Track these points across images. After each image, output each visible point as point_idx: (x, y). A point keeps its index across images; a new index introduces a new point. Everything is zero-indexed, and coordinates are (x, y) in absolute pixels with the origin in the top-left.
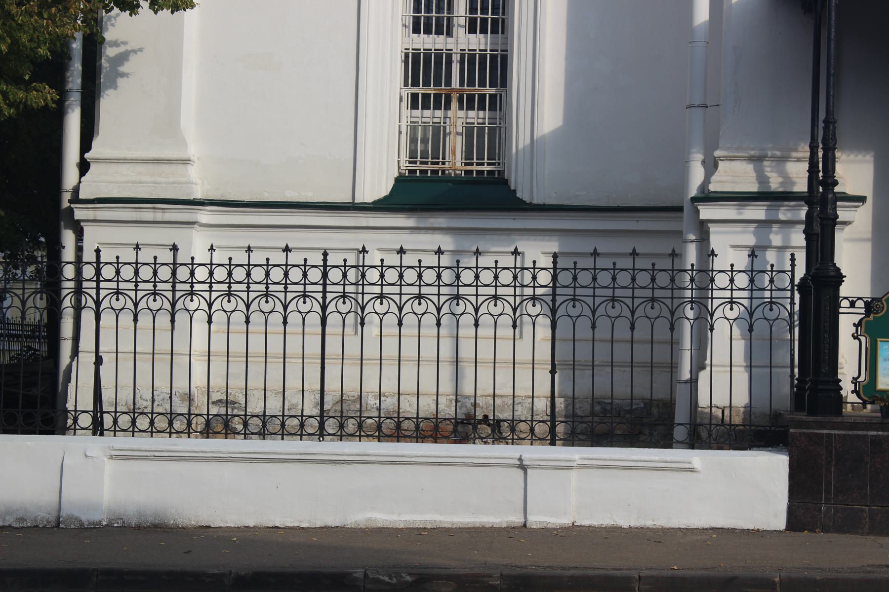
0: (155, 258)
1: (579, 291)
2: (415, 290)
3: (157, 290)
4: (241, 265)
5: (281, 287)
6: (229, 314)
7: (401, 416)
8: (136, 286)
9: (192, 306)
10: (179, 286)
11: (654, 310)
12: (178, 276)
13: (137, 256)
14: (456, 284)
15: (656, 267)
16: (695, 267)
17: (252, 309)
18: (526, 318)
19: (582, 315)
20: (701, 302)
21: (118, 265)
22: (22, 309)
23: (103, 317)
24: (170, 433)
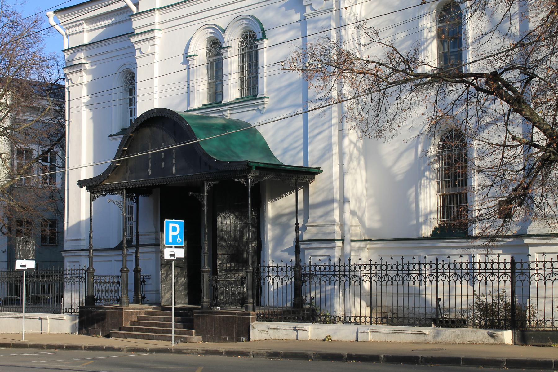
1: (494, 271)
8: (381, 272)
23: (404, 283)
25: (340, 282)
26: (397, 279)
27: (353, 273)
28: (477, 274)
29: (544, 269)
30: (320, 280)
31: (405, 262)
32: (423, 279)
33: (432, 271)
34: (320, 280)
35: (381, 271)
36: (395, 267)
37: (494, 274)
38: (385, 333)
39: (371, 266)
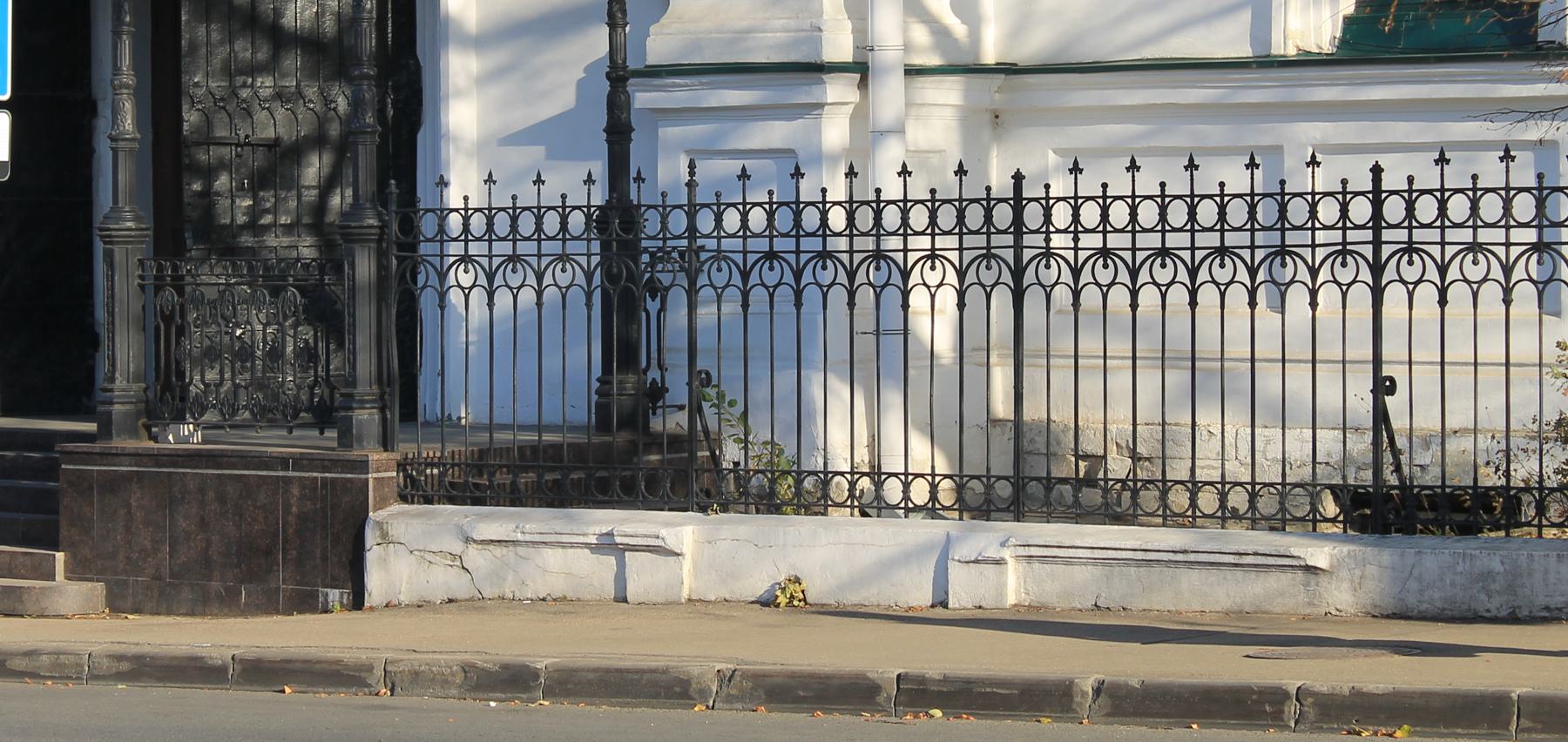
0: (1105, 186)
4: (1494, 190)
7: (1448, 483)
8: (1076, 240)
9: (826, 277)
10: (1386, 235)
11: (1479, 266)
13: (1133, 181)
14: (1309, 225)
15: (938, 196)
16: (775, 196)
17: (1451, 276)
20: (946, 255)
21: (1410, 198)
24: (1224, 519)
26: (1223, 276)
31: (550, 196)
33: (1352, 236)
35: (1076, 232)
39: (1377, 197)
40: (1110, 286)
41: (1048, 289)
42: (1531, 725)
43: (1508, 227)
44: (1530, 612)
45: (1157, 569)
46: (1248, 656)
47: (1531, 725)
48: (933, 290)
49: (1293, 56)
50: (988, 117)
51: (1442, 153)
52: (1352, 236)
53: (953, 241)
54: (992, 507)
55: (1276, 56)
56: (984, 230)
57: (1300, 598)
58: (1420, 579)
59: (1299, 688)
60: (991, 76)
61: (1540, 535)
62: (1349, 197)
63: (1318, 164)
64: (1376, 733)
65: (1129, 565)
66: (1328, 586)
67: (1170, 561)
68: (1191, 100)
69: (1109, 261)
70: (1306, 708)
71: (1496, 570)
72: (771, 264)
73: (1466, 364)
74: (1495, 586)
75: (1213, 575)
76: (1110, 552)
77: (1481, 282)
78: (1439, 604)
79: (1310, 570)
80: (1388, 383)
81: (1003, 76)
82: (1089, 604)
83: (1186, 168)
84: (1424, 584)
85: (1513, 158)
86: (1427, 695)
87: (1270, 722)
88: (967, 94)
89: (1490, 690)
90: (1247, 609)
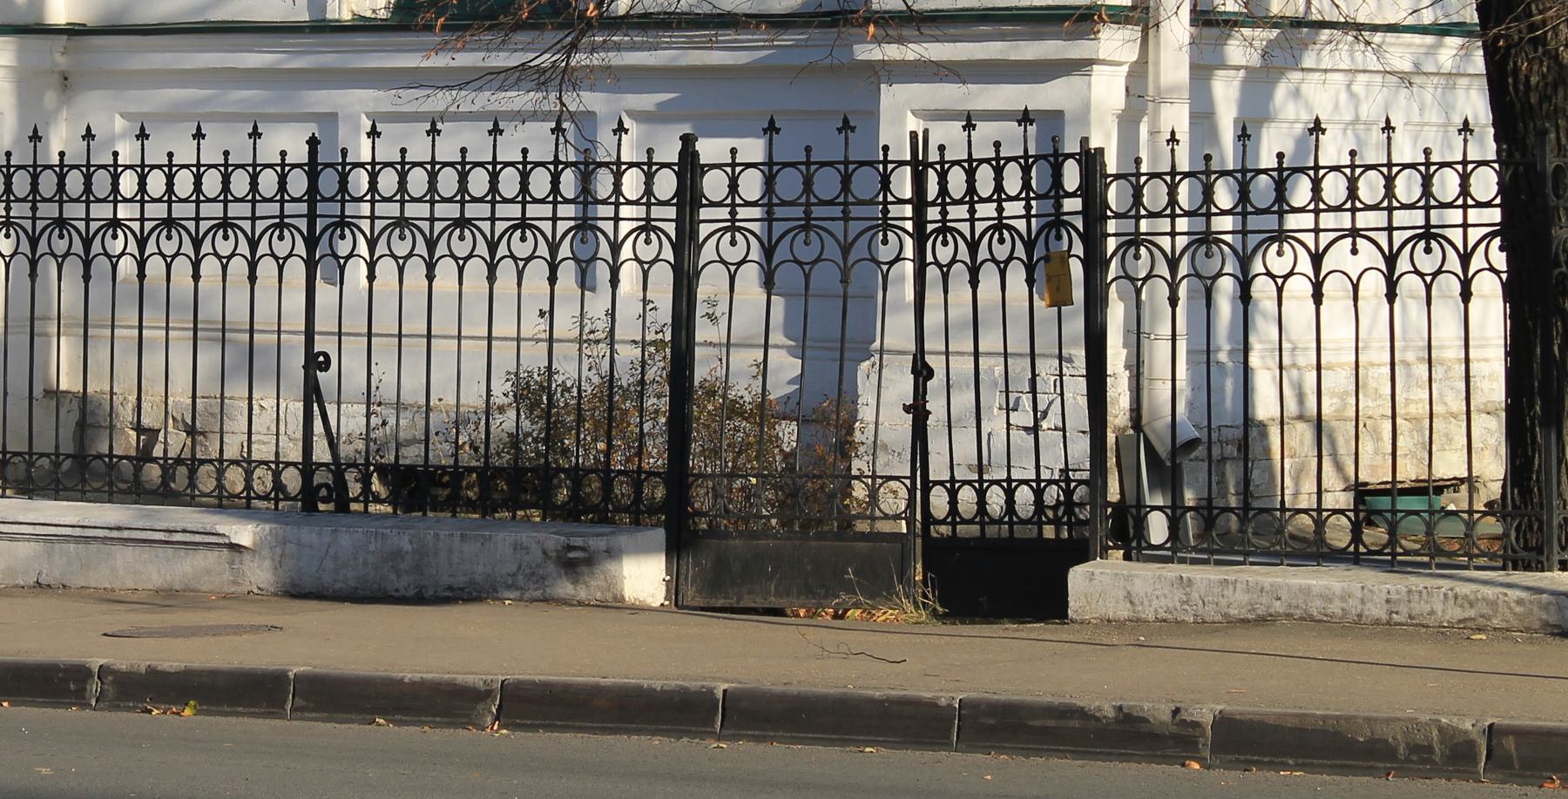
0: (170, 155)
2: (1345, 220)
3: (951, 221)
5: (837, 211)
6: (733, 268)
8: (34, 209)
10: (321, 208)
12: (778, 188)
13: (433, 146)
18: (990, 266)
19: (871, 255)
22: (489, 261)
25: (87, 264)
26: (282, 249)
27: (274, 208)
28: (1410, 233)
29: (808, 204)
30: (34, 247)
32: (605, 250)
33: (656, 212)
34: (34, 247)
35: (34, 202)
36: (448, 182)
37: (1435, 237)
38: (37, 537)
40: (174, 257)
41: (114, 260)
42: (304, 703)
43: (432, 202)
44: (436, 592)
45: (94, 547)
46: (105, 635)
47: (304, 703)
48: (521, 264)
49: (347, 21)
50: (56, 78)
51: (496, 124)
52: (656, 212)
53: (365, 209)
54: (61, 487)
55: (330, 21)
56: (398, 197)
57: (225, 576)
58: (335, 558)
59: (101, 666)
60: (52, 36)
61: (276, 508)
62: (287, 168)
63: (778, 131)
64: (165, 713)
65: (69, 542)
66: (251, 564)
67: (105, 538)
68: (1029, 57)
69: (65, 232)
70: (106, 687)
71: (405, 549)
72: (462, 233)
73: (391, 335)
74: (403, 566)
75: (145, 553)
76: (50, 528)
77: (652, 263)
78: (352, 584)
79: (235, 548)
80: (321, 359)
81: (66, 37)
82: (32, 581)
83: (250, 136)
84: (339, 563)
85: (439, 132)
86: (214, 673)
87: (74, 701)
88: (21, 53)
89: (271, 668)
90: (177, 587)
